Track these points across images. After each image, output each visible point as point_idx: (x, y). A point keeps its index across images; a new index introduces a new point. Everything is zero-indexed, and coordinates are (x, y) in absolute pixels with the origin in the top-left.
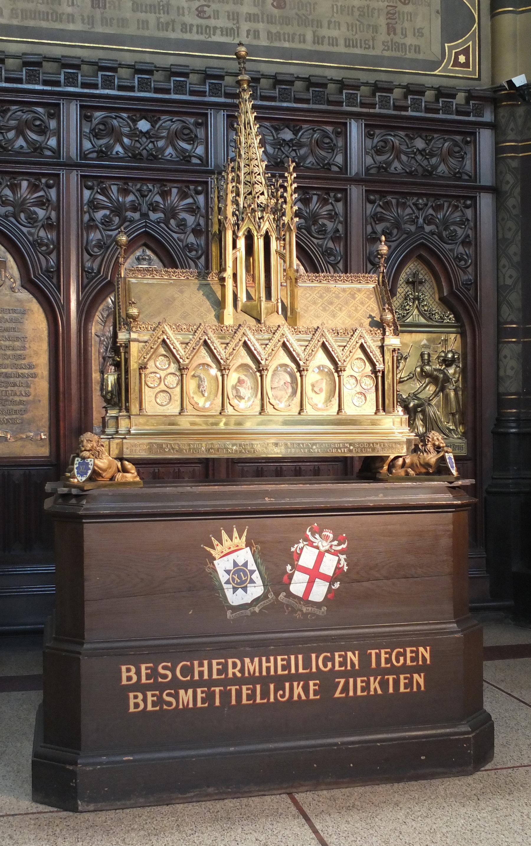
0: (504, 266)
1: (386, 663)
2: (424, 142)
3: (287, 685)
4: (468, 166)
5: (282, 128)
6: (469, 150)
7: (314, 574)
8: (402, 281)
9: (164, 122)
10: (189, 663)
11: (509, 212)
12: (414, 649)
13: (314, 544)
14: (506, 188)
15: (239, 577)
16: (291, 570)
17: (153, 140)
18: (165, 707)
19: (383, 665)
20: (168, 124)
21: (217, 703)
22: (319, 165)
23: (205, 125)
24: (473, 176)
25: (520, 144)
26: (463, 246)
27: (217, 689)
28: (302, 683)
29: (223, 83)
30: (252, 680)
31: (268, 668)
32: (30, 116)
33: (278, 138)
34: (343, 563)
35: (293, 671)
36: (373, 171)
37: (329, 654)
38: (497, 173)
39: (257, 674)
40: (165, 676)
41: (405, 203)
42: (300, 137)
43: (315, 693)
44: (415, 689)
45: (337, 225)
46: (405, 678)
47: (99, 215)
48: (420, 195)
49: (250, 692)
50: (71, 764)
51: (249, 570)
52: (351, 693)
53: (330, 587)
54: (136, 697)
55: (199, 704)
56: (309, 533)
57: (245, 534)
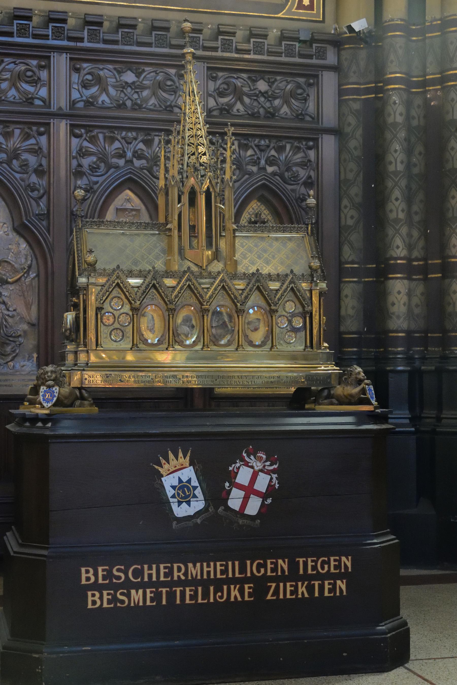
0: (346, 207)
1: (313, 570)
2: (266, 84)
3: (225, 587)
4: (311, 107)
5: (124, 70)
6: (312, 92)
7: (249, 490)
8: (245, 220)
9: (7, 65)
10: (139, 567)
11: (349, 152)
12: (337, 558)
13: (249, 464)
14: (348, 130)
15: (184, 492)
16: (229, 487)
17: (138, 90)
18: (119, 605)
19: (310, 572)
20: (150, 76)
21: (164, 602)
22: (161, 107)
23: (48, 67)
24: (316, 118)
25: (362, 87)
26: (305, 187)
27: (164, 590)
28: (238, 586)
29: (66, 27)
30: (194, 582)
31: (209, 573)
32: (23, 67)
33: (121, 80)
34: (274, 480)
35: (230, 575)
36: (215, 113)
37: (262, 561)
38: (341, 116)
39: (199, 577)
40: (119, 578)
41: (246, 145)
42: (143, 80)
43: (250, 595)
44: (338, 594)
45: (310, 172)
46: (329, 584)
47: (86, 162)
48: (262, 137)
49: (192, 593)
50: (37, 653)
51: (192, 486)
52: (281, 597)
53: (263, 503)
54: (93, 595)
55: (148, 603)
56: (245, 455)
57: (189, 454)
